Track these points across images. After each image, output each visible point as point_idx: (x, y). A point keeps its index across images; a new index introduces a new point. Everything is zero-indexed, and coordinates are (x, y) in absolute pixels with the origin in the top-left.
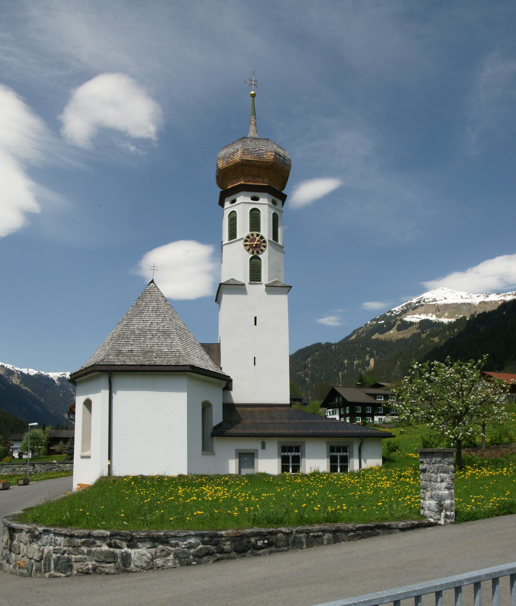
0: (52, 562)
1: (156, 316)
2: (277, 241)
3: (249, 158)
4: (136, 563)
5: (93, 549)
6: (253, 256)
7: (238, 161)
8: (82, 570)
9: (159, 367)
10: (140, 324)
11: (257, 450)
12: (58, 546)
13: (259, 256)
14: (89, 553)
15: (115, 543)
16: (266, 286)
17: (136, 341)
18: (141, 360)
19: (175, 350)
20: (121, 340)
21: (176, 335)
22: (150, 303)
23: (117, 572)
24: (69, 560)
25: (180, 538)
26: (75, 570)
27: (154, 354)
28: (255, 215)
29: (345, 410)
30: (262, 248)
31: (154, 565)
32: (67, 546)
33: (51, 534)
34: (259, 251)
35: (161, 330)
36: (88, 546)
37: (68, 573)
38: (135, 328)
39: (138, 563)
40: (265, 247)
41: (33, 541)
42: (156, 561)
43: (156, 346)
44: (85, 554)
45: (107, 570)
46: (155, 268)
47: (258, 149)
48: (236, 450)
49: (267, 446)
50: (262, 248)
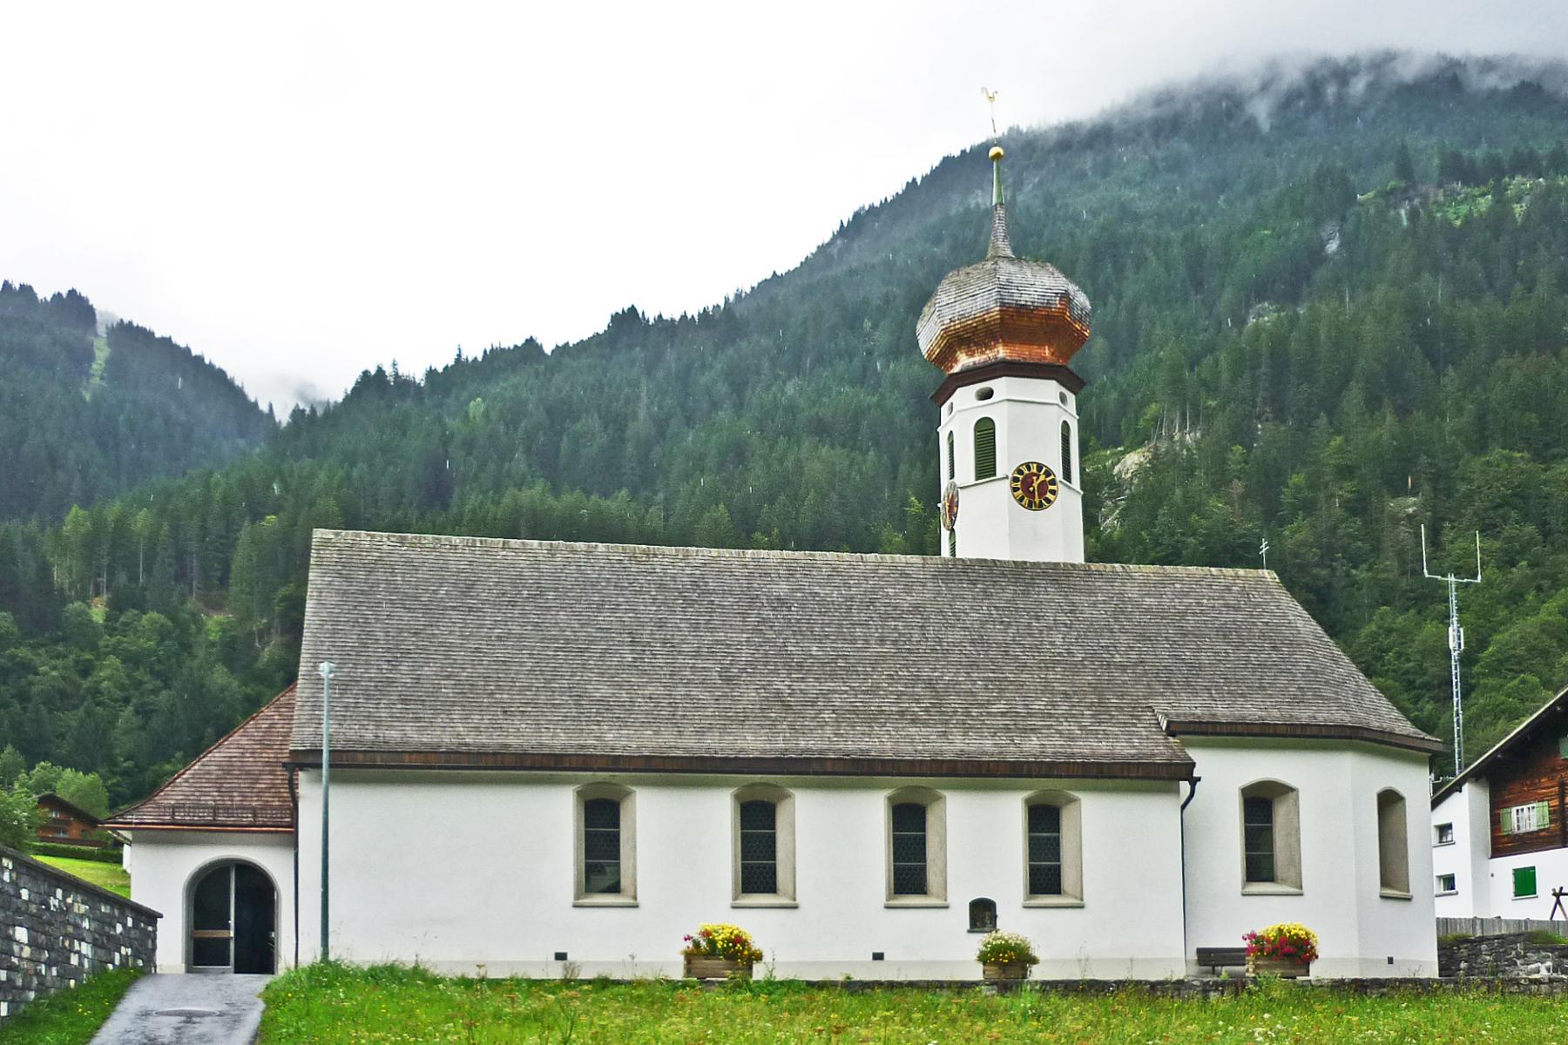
30: (1049, 495)
50: (1049, 495)
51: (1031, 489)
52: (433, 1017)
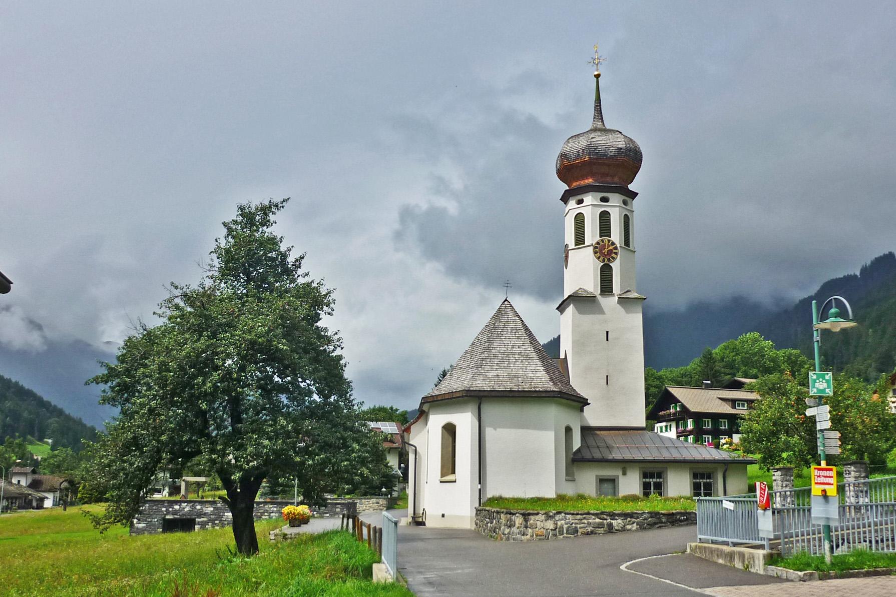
2: (629, 247)
10: (501, 347)
11: (618, 476)
13: (611, 264)
18: (510, 386)
22: (507, 324)
27: (519, 379)
28: (605, 218)
29: (685, 425)
30: (613, 255)
33: (562, 514)
35: (523, 354)
37: (575, 535)
39: (616, 528)
40: (616, 254)
41: (548, 519)
43: (521, 370)
46: (508, 285)
48: (596, 476)
49: (628, 473)
50: (613, 255)
51: (604, 251)
52: (874, 355)
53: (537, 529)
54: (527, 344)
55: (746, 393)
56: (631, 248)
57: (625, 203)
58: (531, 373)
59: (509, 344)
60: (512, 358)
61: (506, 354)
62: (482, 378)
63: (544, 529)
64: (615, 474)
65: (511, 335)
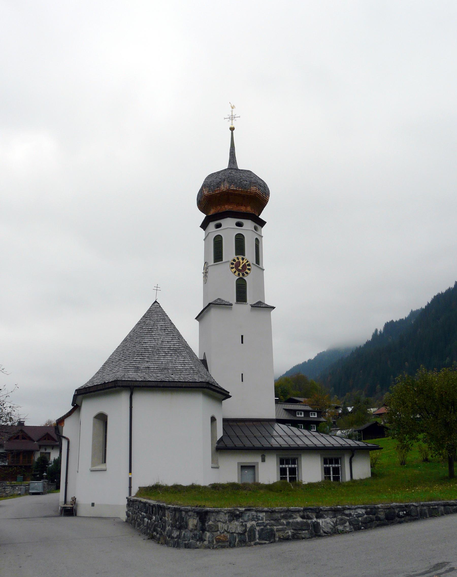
0: (257, 533)
1: (166, 334)
3: (233, 187)
4: (324, 529)
5: (291, 521)
6: (238, 278)
7: (224, 190)
8: (284, 537)
9: (178, 383)
10: (152, 342)
12: (261, 520)
14: (288, 523)
15: (308, 516)
16: (251, 306)
17: (151, 358)
19: (189, 368)
20: (136, 357)
21: (186, 353)
23: (310, 537)
24: (272, 530)
25: (352, 510)
26: (277, 537)
28: (240, 240)
30: (247, 271)
31: (336, 530)
32: (269, 520)
34: (245, 273)
35: (172, 349)
36: (286, 519)
37: (272, 540)
38: (147, 345)
39: (326, 530)
41: (233, 520)
42: (337, 528)
43: (170, 363)
44: (285, 525)
45: (303, 536)
47: (243, 180)
49: (267, 459)
50: (247, 271)
53: (219, 532)
54: (176, 340)
55: (302, 406)
56: (260, 266)
57: (256, 228)
58: (180, 365)
59: (159, 340)
60: (162, 352)
61: (156, 348)
62: (134, 370)
63: (228, 532)
64: (255, 461)
65: (161, 332)
